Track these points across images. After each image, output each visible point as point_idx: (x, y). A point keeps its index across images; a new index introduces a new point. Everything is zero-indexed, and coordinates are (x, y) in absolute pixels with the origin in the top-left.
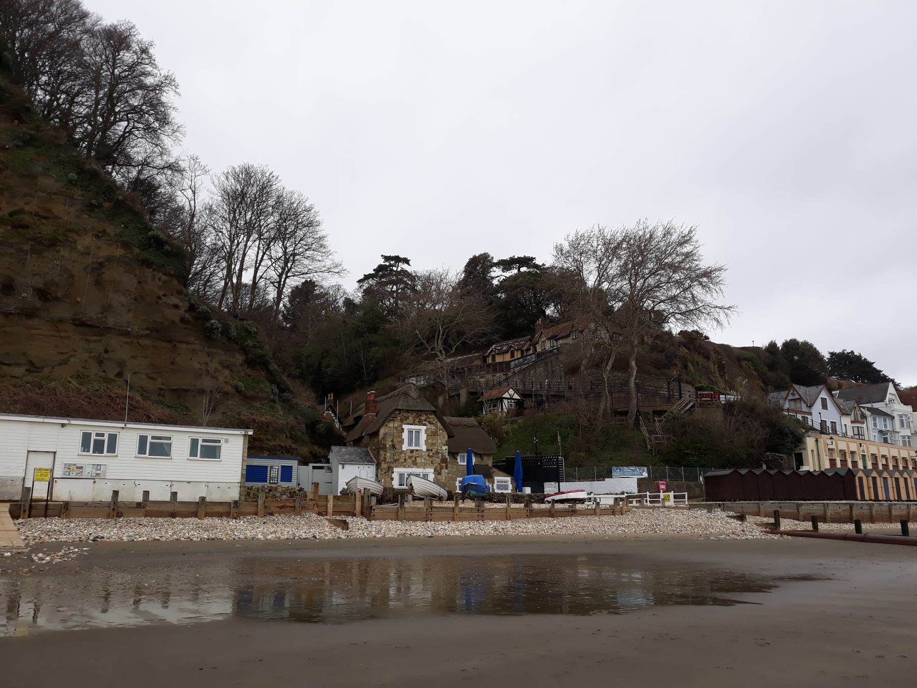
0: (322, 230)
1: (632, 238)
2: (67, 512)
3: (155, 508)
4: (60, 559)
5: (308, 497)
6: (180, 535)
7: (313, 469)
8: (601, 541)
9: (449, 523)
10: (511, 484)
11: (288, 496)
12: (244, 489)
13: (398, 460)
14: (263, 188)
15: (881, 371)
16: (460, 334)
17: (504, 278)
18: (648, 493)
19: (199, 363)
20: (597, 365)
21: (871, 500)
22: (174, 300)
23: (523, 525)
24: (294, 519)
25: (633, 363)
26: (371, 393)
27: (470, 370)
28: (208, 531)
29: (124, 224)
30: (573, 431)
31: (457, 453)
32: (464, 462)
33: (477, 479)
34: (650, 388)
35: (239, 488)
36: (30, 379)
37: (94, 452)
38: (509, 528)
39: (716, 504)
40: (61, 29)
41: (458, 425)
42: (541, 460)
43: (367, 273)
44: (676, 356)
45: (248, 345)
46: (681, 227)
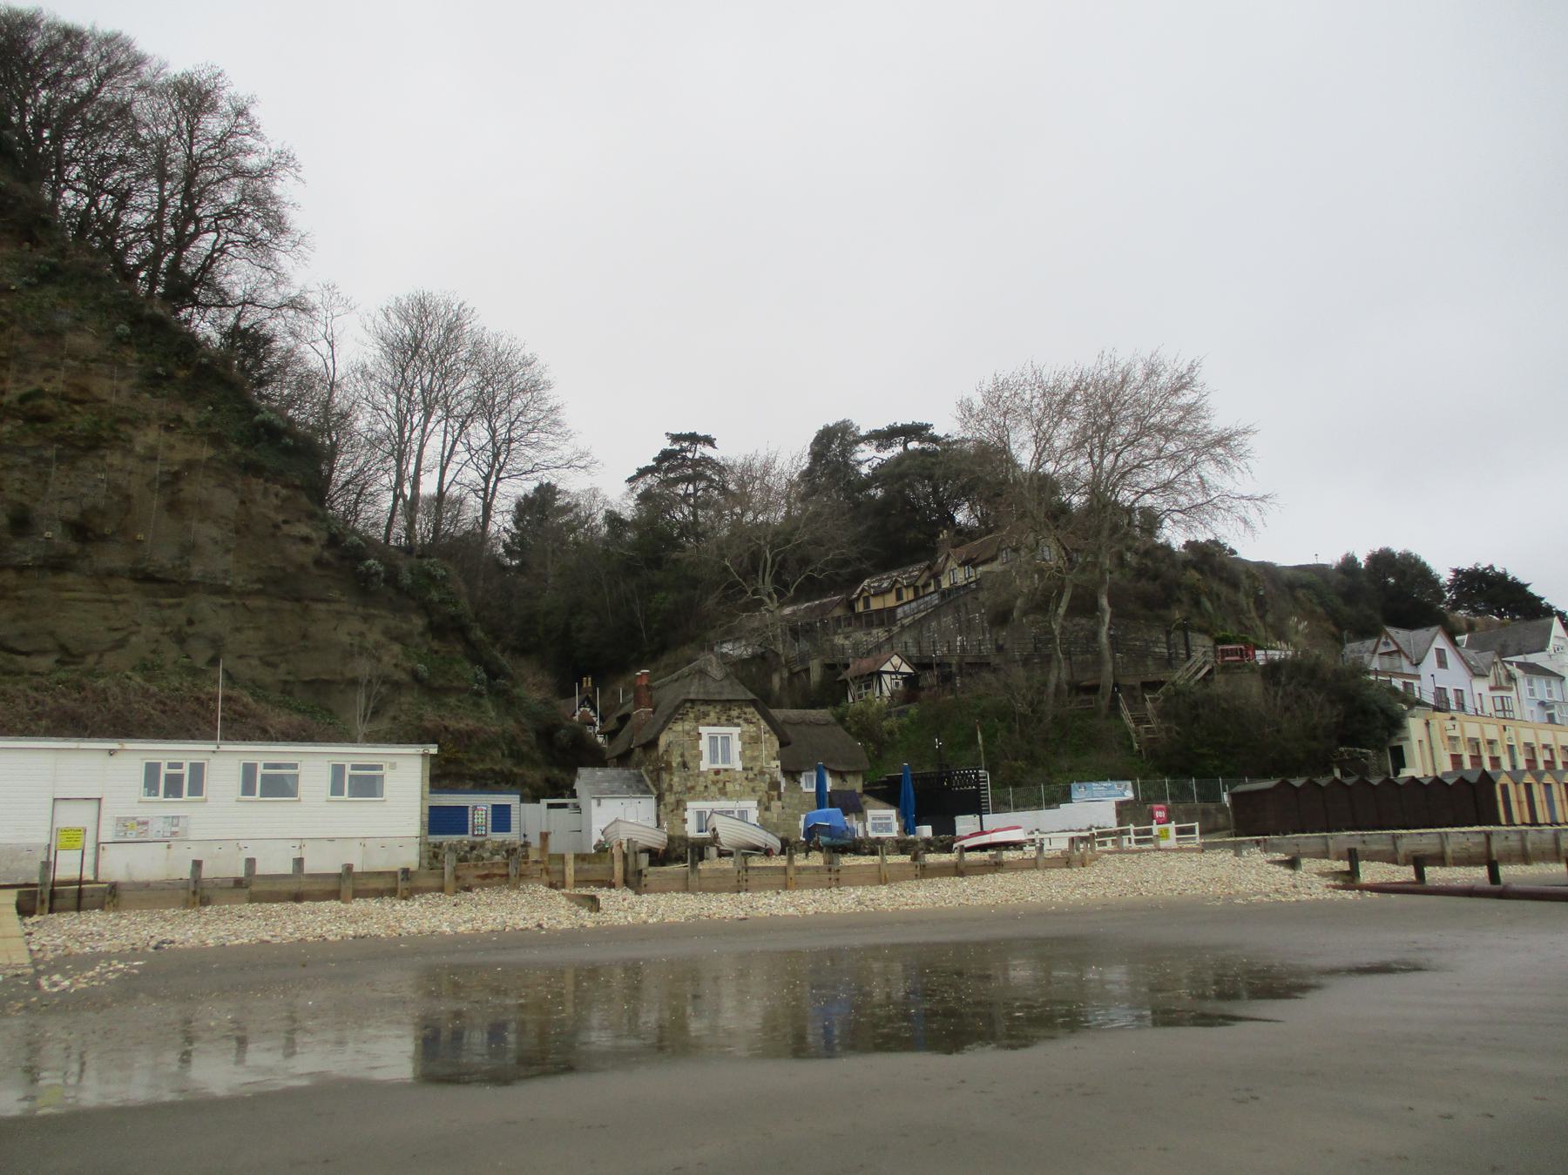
0: (553, 397)
2: (115, 901)
3: (266, 887)
4: (87, 983)
6: (307, 931)
8: (1041, 914)
9: (778, 893)
13: (693, 788)
14: (450, 330)
15: (1542, 599)
16: (804, 562)
18: (1132, 827)
19: (349, 634)
20: (1042, 604)
21: (1524, 824)
22: (303, 529)
23: (907, 893)
24: (507, 896)
25: (1104, 602)
27: (824, 626)
29: (212, 404)
31: (800, 773)
33: (832, 816)
36: (62, 675)
37: (166, 796)
38: (883, 898)
39: (1252, 840)
40: (100, 85)
42: (949, 778)
43: (642, 466)
44: (1179, 586)
45: (431, 601)
46: (1174, 361)
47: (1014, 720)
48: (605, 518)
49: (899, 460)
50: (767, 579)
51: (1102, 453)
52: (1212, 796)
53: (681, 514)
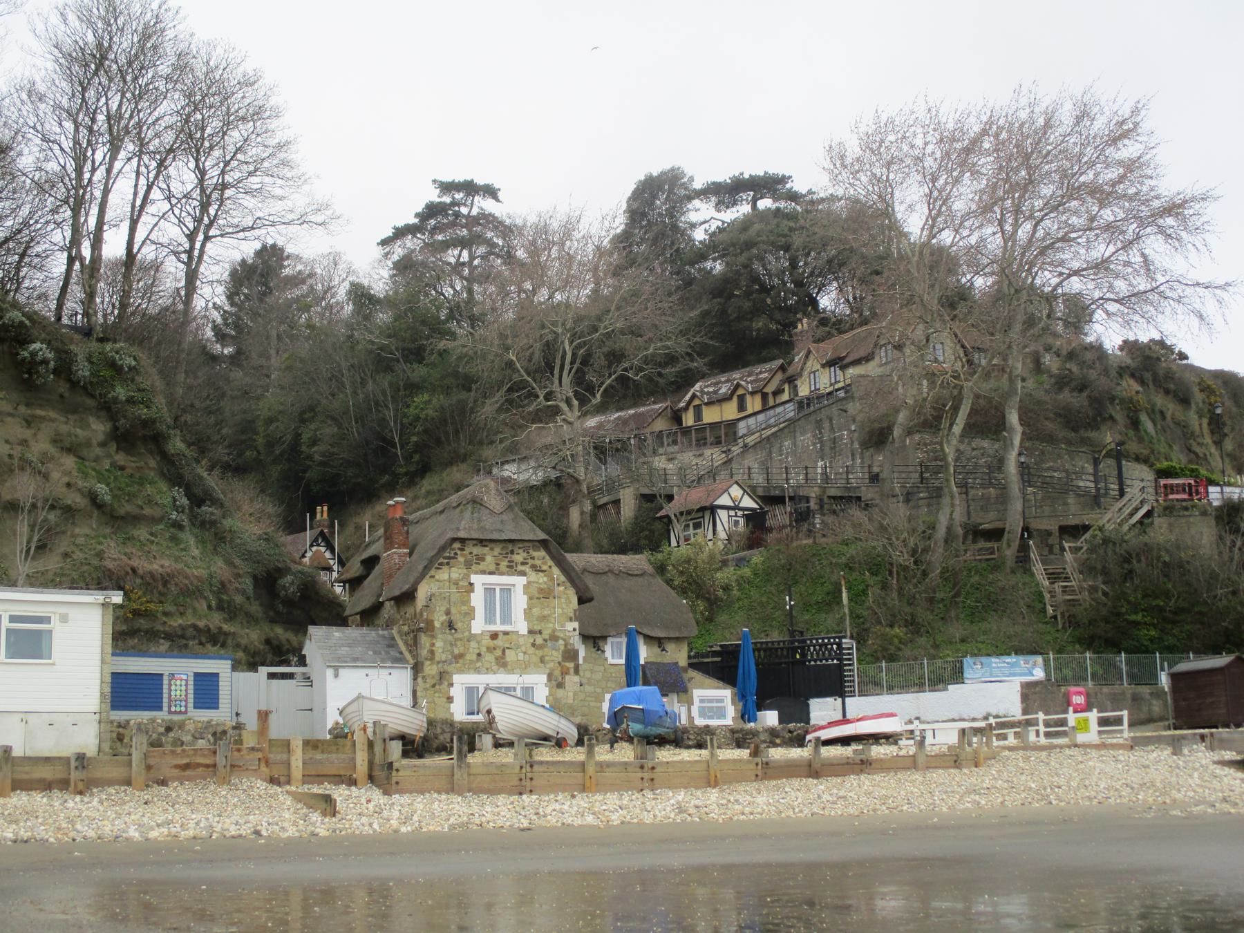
0: (281, 129)
1: (1003, 128)
5: (245, 743)
7: (268, 678)
8: (920, 828)
9: (573, 796)
10: (733, 704)
11: (209, 741)
12: (108, 727)
13: (461, 656)
16: (615, 357)
17: (720, 224)
18: (1041, 716)
19: (7, 442)
24: (213, 793)
25: (1013, 418)
26: (397, 502)
27: (641, 441)
28: (16, 822)
30: (879, 578)
31: (604, 638)
32: (621, 657)
33: (647, 697)
34: (1056, 474)
35: (97, 725)
39: (1195, 734)
41: (605, 573)
42: (802, 648)
43: (400, 224)
45: (115, 399)
47: (891, 573)
48: (349, 293)
49: (744, 225)
50: (566, 379)
51: (1016, 220)
52: (1146, 677)
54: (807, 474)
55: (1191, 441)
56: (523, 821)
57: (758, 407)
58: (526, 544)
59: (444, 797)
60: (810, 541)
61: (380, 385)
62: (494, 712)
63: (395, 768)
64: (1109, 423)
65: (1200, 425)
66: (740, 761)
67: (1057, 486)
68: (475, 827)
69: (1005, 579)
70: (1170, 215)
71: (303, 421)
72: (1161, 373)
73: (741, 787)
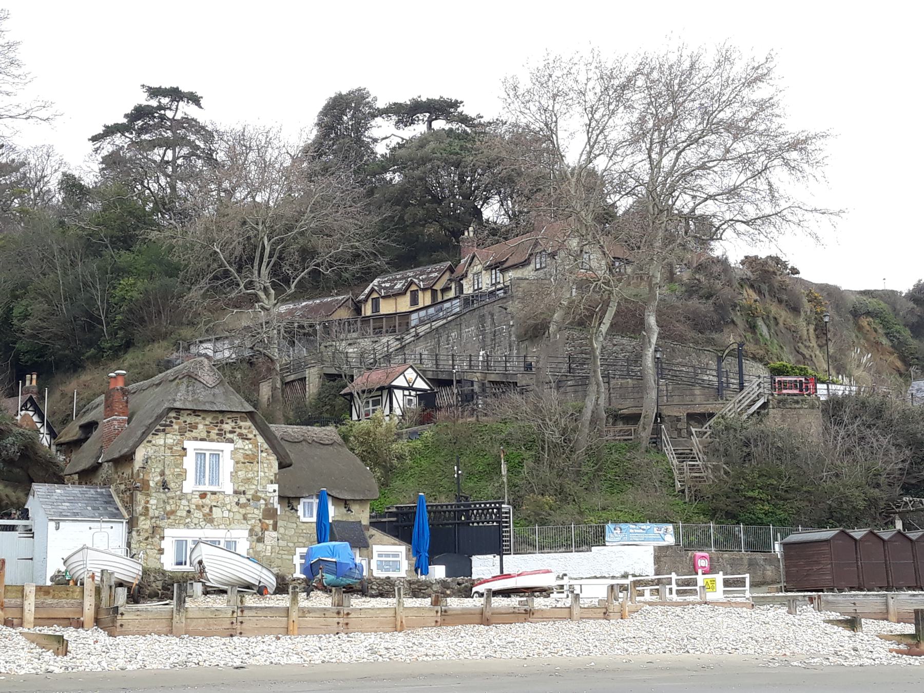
9: (278, 638)
13: (173, 512)
16: (307, 254)
17: (400, 141)
18: (674, 576)
23: (427, 642)
25: (652, 320)
26: (118, 375)
27: (327, 329)
31: (298, 499)
39: (804, 596)
44: (734, 306)
47: (543, 449)
48: (61, 183)
49: (422, 142)
50: (264, 271)
51: (661, 150)
52: (760, 546)
53: (156, 185)
54: (470, 361)
55: (800, 344)
56: (235, 660)
57: (428, 302)
58: (235, 415)
59: (163, 638)
60: (473, 419)
61: (88, 268)
62: (205, 563)
63: (120, 612)
64: (732, 326)
65: (808, 330)
66: (423, 608)
67: (684, 379)
68: (194, 666)
69: (640, 458)
70: (795, 150)
71: (16, 297)
72: (776, 285)
73: (422, 632)
